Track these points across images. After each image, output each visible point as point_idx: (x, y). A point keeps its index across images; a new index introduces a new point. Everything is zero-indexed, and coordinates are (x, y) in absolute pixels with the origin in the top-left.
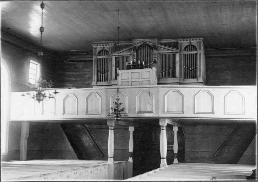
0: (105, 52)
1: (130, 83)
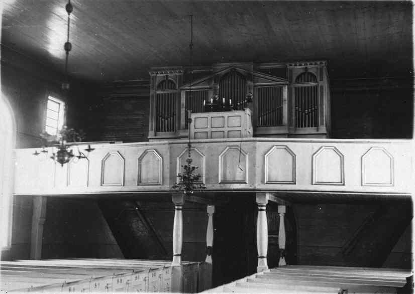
1: (209, 134)
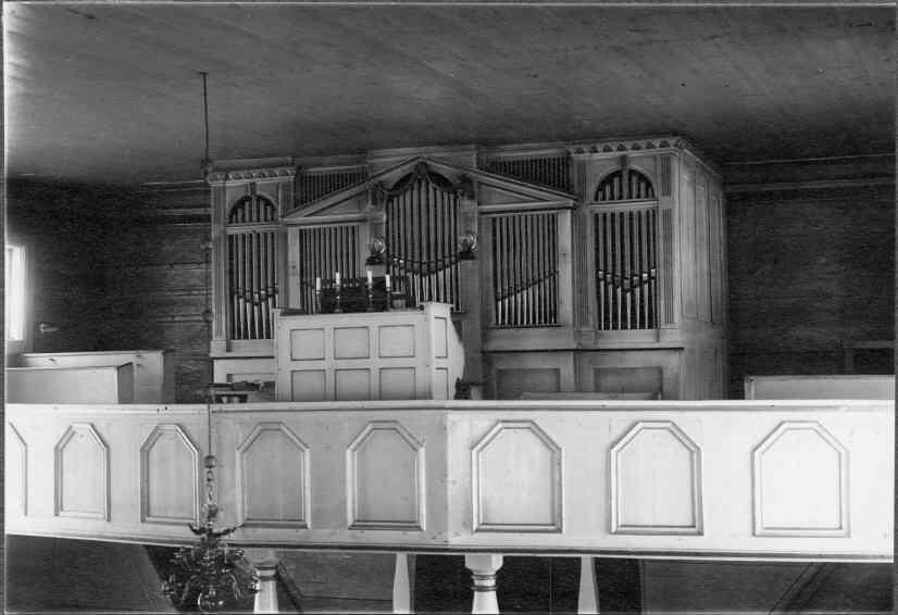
0: (630, 180)
